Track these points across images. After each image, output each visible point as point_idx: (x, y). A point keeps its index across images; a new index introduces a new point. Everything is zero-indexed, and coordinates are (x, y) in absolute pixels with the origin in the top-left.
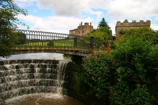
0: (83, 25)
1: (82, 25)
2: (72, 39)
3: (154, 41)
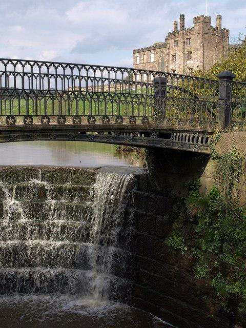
0: (186, 27)
1: (183, 26)
2: (103, 88)
3: (194, 112)
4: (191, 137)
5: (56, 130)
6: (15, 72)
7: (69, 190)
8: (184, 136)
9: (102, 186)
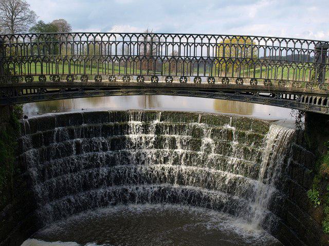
4: (309, 98)
5: (178, 88)
6: (202, 43)
7: (249, 136)
8: (313, 99)
9: (274, 133)
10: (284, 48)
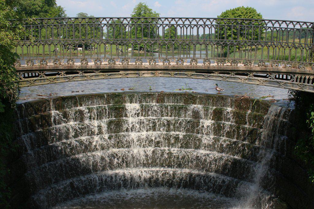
10: (195, 25)
